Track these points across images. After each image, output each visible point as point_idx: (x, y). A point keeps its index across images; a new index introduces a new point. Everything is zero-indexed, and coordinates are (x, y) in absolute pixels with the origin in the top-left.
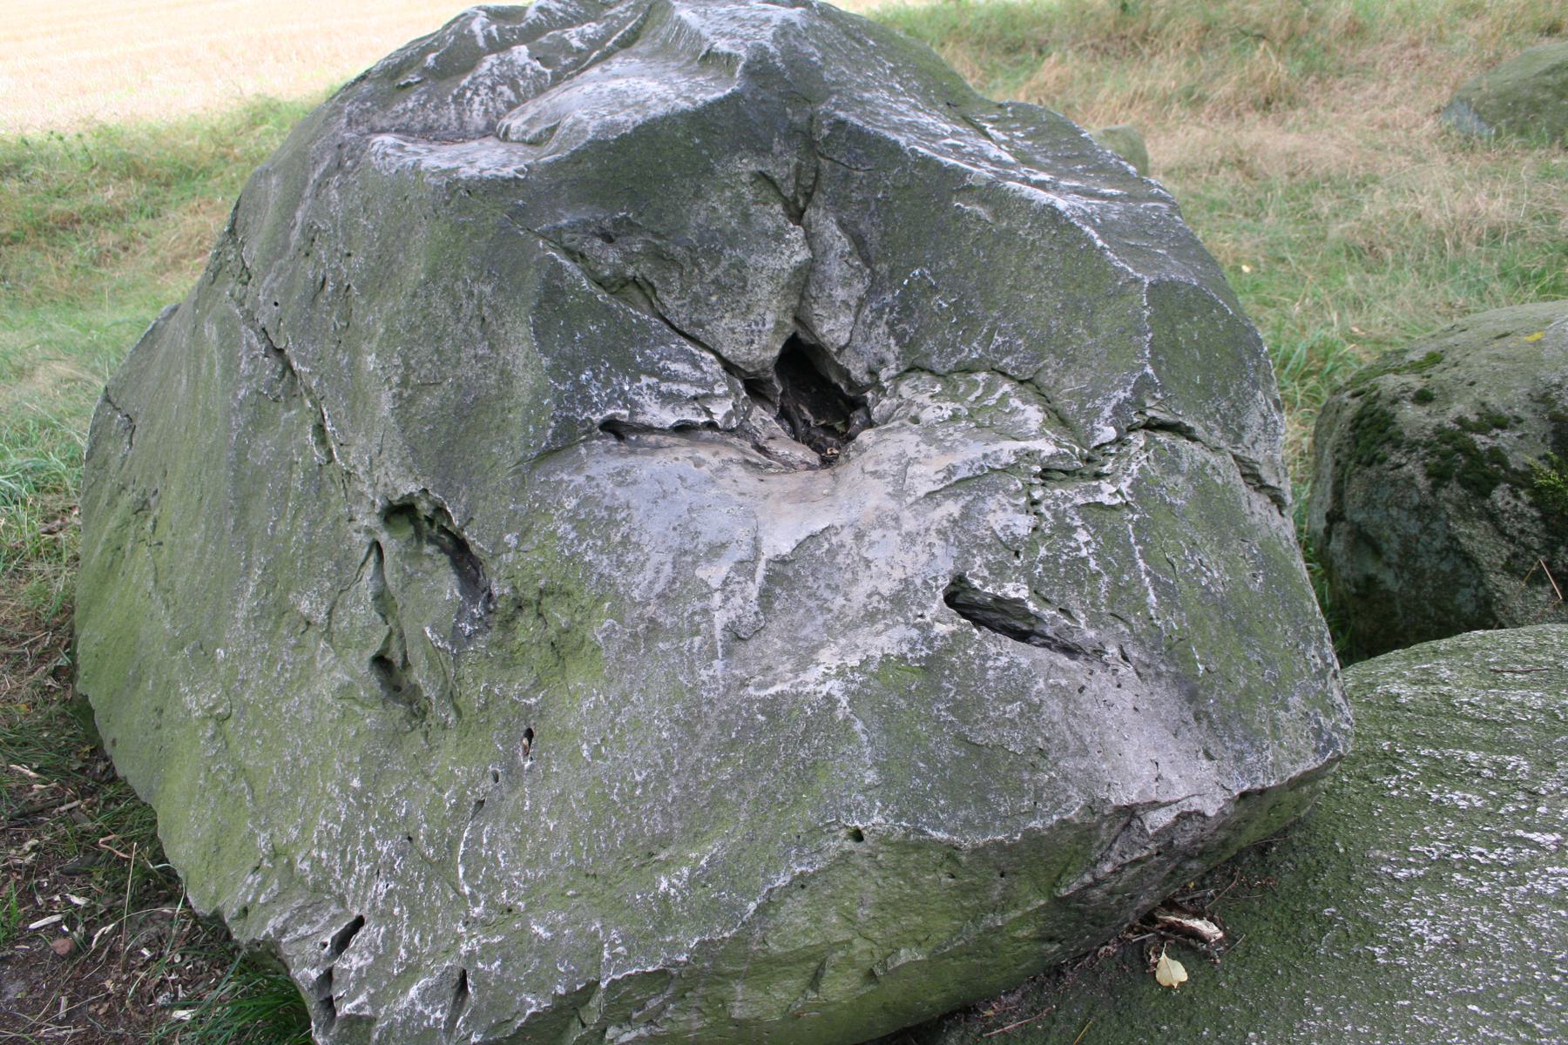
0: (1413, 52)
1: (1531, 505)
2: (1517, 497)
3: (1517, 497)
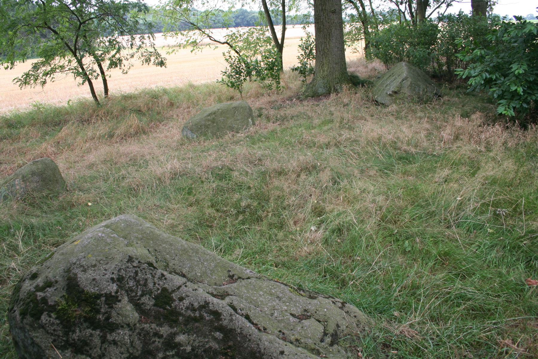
0: (188, 110)
1: (56, 318)
2: (50, 317)
3: (50, 317)
